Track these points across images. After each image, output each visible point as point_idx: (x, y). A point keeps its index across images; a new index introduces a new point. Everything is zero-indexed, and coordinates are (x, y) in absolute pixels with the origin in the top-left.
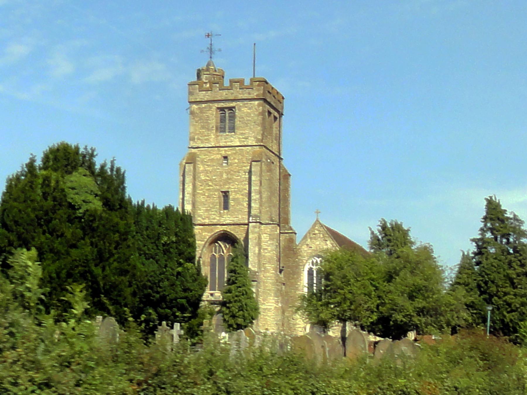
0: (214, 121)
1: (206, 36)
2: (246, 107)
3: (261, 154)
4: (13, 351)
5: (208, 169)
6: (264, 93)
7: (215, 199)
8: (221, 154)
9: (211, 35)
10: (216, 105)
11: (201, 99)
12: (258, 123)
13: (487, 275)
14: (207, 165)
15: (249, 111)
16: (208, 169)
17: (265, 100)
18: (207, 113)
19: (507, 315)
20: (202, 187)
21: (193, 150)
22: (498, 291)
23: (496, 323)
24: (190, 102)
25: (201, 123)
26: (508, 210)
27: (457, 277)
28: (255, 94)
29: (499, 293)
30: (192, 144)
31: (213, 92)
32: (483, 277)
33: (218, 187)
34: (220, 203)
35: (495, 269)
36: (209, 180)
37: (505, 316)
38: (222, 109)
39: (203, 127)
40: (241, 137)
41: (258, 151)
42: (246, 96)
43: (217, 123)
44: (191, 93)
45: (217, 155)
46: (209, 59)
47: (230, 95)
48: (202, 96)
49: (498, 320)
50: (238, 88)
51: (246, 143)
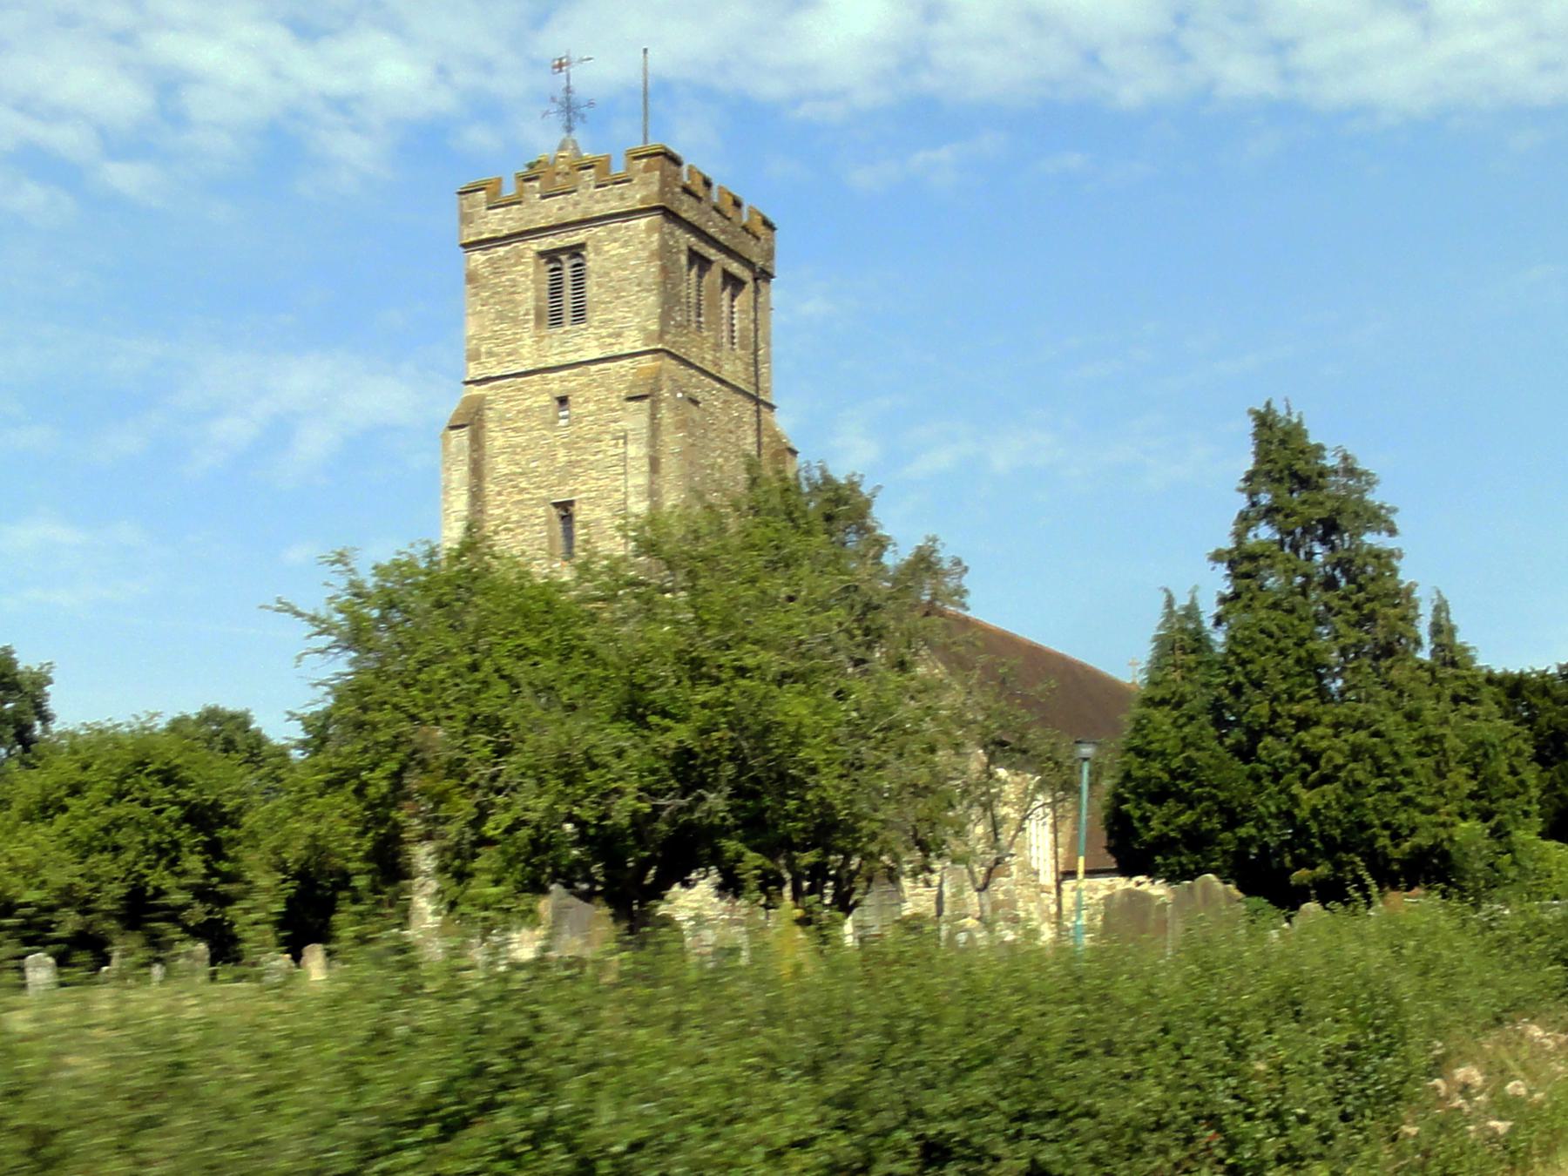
0: (529, 294)
1: (554, 67)
2: (615, 241)
3: (657, 376)
4: (414, 1001)
5: (519, 439)
6: (662, 192)
7: (537, 528)
8: (549, 391)
9: (568, 64)
10: (536, 245)
11: (494, 231)
12: (649, 284)
13: (1243, 663)
14: (514, 430)
15: (622, 251)
16: (519, 439)
17: (670, 214)
18: (509, 273)
19: (1304, 795)
20: (502, 498)
21: (476, 390)
22: (1275, 716)
23: (1266, 826)
24: (464, 246)
25: (495, 304)
26: (1327, 445)
27: (1154, 683)
28: (638, 196)
29: (1279, 723)
30: (474, 371)
31: (524, 206)
32: (1230, 671)
33: (544, 493)
34: (552, 540)
35: (1270, 642)
36: (521, 474)
37: (1294, 799)
38: (550, 256)
39: (501, 317)
40: (604, 332)
41: (648, 368)
42: (615, 206)
43: (538, 299)
44: (466, 219)
45: (539, 396)
46: (565, 135)
47: (571, 208)
48: (497, 222)
49: (1271, 815)
50: (593, 183)
51: (616, 350)
